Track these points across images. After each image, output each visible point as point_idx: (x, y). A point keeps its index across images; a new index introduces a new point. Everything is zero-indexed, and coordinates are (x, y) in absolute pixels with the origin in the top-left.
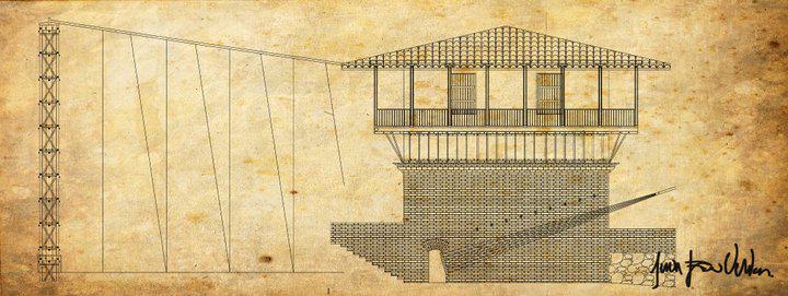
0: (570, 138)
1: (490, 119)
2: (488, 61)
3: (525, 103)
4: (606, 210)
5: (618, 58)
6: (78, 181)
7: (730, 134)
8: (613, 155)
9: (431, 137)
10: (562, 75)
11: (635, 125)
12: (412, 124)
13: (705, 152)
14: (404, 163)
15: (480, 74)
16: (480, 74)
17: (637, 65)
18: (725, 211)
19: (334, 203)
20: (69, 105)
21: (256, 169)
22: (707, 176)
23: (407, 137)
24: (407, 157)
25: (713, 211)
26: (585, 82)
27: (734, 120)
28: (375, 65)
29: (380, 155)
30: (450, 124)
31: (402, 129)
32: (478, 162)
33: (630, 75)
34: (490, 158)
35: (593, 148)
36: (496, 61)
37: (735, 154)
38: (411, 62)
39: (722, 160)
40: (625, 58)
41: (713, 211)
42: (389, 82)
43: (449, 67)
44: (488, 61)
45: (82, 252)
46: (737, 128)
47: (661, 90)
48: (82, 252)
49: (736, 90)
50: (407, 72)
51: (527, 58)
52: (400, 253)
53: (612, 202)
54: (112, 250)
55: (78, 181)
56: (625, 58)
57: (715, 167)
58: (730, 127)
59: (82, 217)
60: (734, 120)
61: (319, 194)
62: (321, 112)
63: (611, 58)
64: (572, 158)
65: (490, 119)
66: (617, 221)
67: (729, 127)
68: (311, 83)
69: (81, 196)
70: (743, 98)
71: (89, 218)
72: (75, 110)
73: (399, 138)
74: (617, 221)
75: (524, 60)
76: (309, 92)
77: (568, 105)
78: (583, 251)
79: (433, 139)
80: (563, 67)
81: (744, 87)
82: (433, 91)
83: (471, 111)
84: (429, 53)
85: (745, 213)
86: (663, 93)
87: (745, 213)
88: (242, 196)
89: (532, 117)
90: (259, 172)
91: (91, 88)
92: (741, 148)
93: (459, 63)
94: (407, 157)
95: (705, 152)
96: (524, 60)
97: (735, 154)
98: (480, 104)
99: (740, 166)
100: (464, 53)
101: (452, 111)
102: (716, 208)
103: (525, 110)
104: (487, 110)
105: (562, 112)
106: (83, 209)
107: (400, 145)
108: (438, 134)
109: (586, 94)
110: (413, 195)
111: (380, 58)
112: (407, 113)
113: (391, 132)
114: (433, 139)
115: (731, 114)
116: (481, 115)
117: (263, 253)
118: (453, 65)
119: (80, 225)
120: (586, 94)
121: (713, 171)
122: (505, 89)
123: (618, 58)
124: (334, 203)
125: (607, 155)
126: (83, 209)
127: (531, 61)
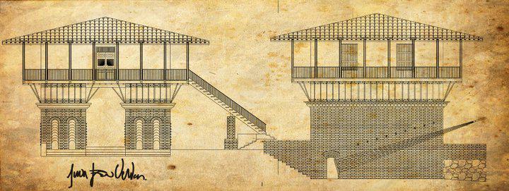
0: (342, 86)
1: (367, 74)
3: (389, 63)
4: (442, 132)
5: (449, 34)
7: (472, 87)
8: (446, 97)
9: (379, 85)
10: (413, 45)
11: (460, 77)
12: (316, 76)
13: (455, 98)
14: (42, 110)
15: (360, 44)
16: (360, 44)
17: (188, 41)
18: (469, 136)
19: (216, 131)
22: (457, 114)
23: (337, 85)
24: (313, 98)
25: (460, 136)
26: (378, 53)
27: (474, 78)
28: (292, 38)
29: (246, 100)
30: (340, 76)
31: (309, 80)
32: (402, 101)
34: (404, 98)
35: (435, 91)
36: (99, 39)
37: (475, 99)
38: (315, 37)
39: (466, 103)
40: (181, 37)
41: (460, 136)
42: (251, 53)
43: (340, 40)
46: (476, 82)
47: (427, 58)
49: (476, 58)
50: (313, 44)
52: (422, 152)
53: (445, 126)
56: (181, 37)
57: (462, 108)
58: (471, 82)
60: (474, 78)
61: (206, 125)
62: (207, 72)
63: (445, 34)
64: (419, 98)
65: (367, 74)
66: (448, 138)
67: (471, 82)
68: (201, 54)
70: (480, 63)
73: (308, 86)
74: (448, 138)
75: (388, 36)
76: (200, 59)
77: (416, 65)
78: (435, 159)
79: (342, 86)
80: (413, 40)
81: (481, 56)
82: (329, 55)
83: (354, 68)
84: (327, 31)
85: (481, 137)
86: (428, 60)
87: (481, 137)
89: (393, 72)
91: (59, 57)
92: (479, 96)
93: (346, 41)
94: (313, 98)
95: (455, 98)
96: (388, 36)
97: (475, 99)
98: (360, 62)
99: (478, 107)
101: (342, 69)
102: (462, 134)
103: (389, 68)
104: (364, 68)
105: (413, 69)
107: (308, 89)
108: (333, 83)
109: (379, 61)
110: (317, 124)
111: (295, 34)
113: (303, 82)
114: (330, 86)
115: (472, 73)
116: (360, 72)
118: (143, 42)
120: (379, 61)
121: (461, 110)
122: (374, 55)
123: (436, 31)
124: (216, 131)
125: (442, 98)
127: (393, 36)
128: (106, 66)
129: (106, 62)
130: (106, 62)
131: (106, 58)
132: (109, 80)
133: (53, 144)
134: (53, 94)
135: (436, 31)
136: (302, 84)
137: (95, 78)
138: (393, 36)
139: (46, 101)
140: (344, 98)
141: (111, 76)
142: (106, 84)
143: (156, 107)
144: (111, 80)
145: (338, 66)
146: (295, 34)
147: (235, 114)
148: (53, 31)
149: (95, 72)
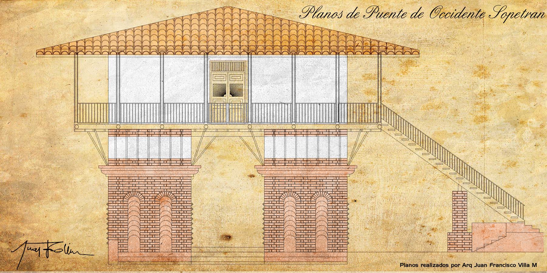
2: (207, 46)
6: (54, 165)
20: (46, 96)
21: (217, 155)
33: (156, 59)
44: (207, 46)
45: (57, 231)
48: (57, 231)
51: (211, 43)
54: (84, 229)
55: (54, 165)
59: (57, 198)
69: (56, 180)
71: (64, 200)
72: (51, 100)
88: (205, 179)
90: (220, 157)
100: (220, 38)
106: (58, 192)
112: (112, 108)
117: (223, 232)
119: (55, 206)
123: (326, 38)
126: (58, 192)
128: (228, 97)
129: (228, 91)
130: (228, 91)
131: (227, 83)
132: (235, 123)
133: (131, 242)
134: (173, 149)
135: (326, 38)
136: (93, 134)
137: (210, 120)
138: (183, 46)
139: (117, 162)
140: (304, 156)
141: (237, 115)
142: (228, 130)
143: (166, 172)
144: (238, 123)
145: (290, 101)
146: (81, 43)
147: (467, 187)
148: (105, 38)
149: (209, 107)
